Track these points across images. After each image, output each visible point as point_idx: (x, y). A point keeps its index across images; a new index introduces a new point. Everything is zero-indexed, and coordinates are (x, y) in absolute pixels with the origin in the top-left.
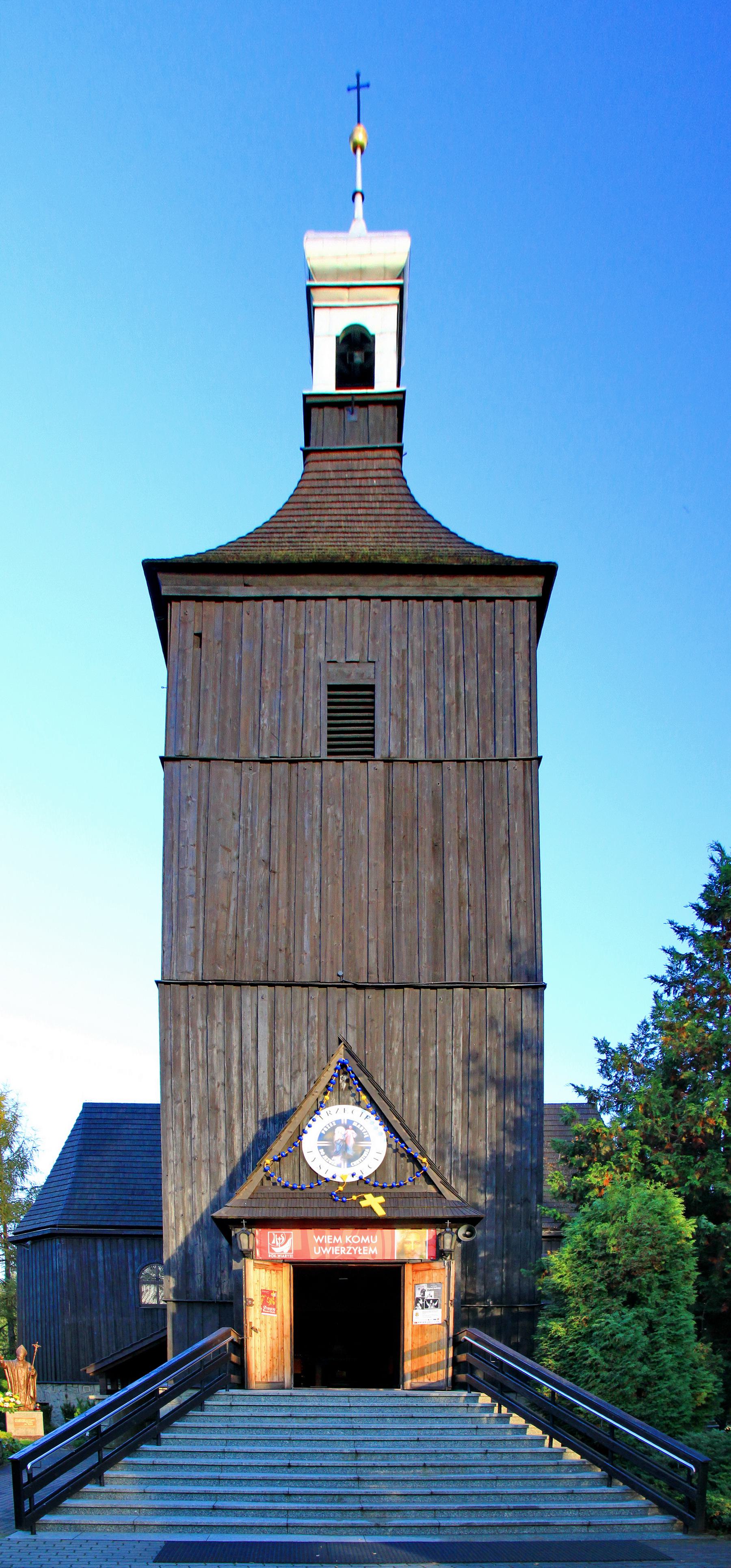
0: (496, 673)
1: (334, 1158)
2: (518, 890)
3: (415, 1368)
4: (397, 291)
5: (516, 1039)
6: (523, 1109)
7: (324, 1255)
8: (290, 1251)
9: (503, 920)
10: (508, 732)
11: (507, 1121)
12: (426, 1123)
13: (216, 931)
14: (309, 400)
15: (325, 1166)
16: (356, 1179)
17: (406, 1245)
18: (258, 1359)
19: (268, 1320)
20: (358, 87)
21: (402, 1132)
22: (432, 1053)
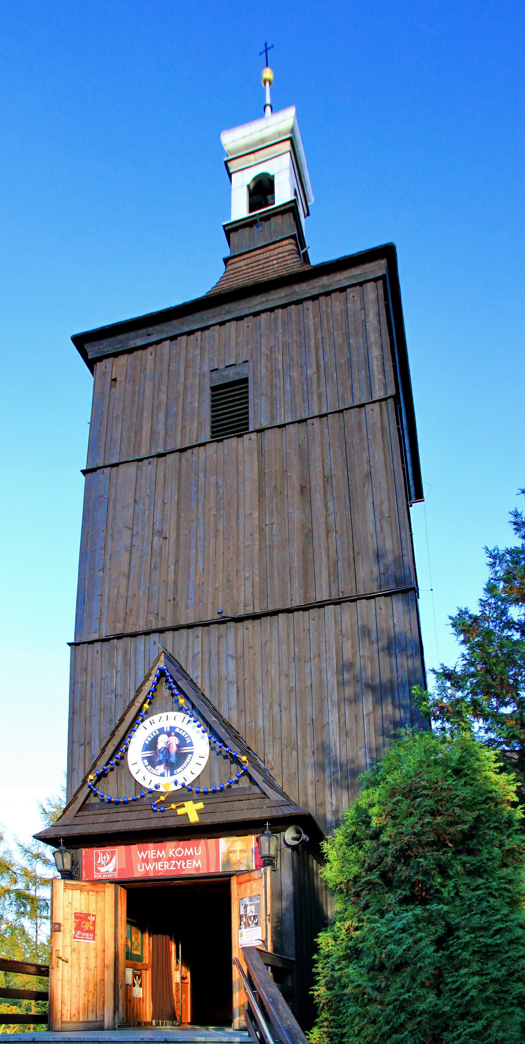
0: (351, 341)
1: (157, 767)
2: (381, 510)
3: (242, 1002)
4: (288, 143)
5: (389, 644)
6: (402, 711)
7: (148, 872)
8: (115, 870)
9: (369, 537)
10: (364, 385)
11: (386, 725)
12: (304, 737)
13: (118, 595)
14: (227, 228)
15: (149, 776)
16: (179, 787)
17: (231, 855)
18: (66, 993)
19: (83, 947)
20: (266, 51)
21: (222, 732)
22: (307, 670)
